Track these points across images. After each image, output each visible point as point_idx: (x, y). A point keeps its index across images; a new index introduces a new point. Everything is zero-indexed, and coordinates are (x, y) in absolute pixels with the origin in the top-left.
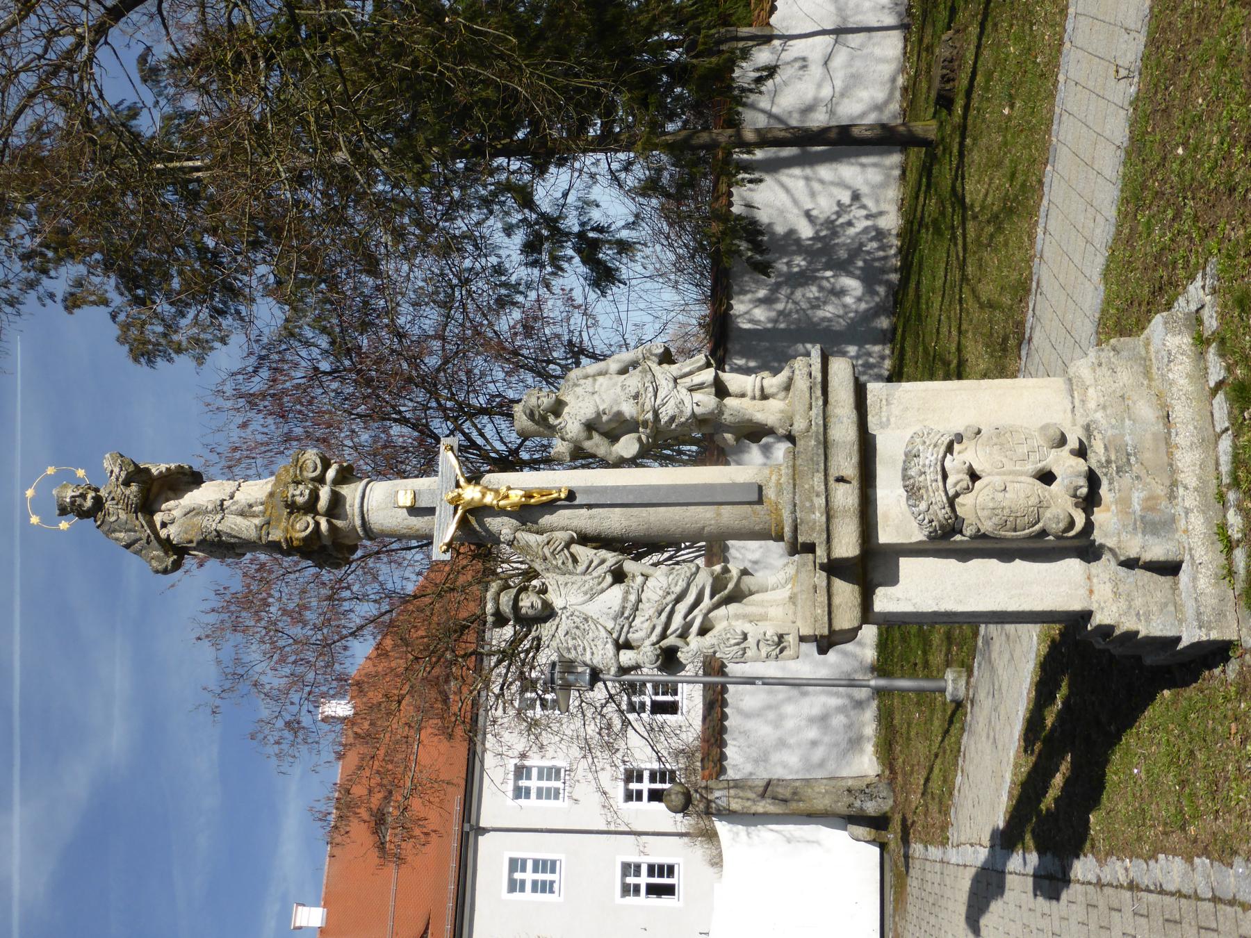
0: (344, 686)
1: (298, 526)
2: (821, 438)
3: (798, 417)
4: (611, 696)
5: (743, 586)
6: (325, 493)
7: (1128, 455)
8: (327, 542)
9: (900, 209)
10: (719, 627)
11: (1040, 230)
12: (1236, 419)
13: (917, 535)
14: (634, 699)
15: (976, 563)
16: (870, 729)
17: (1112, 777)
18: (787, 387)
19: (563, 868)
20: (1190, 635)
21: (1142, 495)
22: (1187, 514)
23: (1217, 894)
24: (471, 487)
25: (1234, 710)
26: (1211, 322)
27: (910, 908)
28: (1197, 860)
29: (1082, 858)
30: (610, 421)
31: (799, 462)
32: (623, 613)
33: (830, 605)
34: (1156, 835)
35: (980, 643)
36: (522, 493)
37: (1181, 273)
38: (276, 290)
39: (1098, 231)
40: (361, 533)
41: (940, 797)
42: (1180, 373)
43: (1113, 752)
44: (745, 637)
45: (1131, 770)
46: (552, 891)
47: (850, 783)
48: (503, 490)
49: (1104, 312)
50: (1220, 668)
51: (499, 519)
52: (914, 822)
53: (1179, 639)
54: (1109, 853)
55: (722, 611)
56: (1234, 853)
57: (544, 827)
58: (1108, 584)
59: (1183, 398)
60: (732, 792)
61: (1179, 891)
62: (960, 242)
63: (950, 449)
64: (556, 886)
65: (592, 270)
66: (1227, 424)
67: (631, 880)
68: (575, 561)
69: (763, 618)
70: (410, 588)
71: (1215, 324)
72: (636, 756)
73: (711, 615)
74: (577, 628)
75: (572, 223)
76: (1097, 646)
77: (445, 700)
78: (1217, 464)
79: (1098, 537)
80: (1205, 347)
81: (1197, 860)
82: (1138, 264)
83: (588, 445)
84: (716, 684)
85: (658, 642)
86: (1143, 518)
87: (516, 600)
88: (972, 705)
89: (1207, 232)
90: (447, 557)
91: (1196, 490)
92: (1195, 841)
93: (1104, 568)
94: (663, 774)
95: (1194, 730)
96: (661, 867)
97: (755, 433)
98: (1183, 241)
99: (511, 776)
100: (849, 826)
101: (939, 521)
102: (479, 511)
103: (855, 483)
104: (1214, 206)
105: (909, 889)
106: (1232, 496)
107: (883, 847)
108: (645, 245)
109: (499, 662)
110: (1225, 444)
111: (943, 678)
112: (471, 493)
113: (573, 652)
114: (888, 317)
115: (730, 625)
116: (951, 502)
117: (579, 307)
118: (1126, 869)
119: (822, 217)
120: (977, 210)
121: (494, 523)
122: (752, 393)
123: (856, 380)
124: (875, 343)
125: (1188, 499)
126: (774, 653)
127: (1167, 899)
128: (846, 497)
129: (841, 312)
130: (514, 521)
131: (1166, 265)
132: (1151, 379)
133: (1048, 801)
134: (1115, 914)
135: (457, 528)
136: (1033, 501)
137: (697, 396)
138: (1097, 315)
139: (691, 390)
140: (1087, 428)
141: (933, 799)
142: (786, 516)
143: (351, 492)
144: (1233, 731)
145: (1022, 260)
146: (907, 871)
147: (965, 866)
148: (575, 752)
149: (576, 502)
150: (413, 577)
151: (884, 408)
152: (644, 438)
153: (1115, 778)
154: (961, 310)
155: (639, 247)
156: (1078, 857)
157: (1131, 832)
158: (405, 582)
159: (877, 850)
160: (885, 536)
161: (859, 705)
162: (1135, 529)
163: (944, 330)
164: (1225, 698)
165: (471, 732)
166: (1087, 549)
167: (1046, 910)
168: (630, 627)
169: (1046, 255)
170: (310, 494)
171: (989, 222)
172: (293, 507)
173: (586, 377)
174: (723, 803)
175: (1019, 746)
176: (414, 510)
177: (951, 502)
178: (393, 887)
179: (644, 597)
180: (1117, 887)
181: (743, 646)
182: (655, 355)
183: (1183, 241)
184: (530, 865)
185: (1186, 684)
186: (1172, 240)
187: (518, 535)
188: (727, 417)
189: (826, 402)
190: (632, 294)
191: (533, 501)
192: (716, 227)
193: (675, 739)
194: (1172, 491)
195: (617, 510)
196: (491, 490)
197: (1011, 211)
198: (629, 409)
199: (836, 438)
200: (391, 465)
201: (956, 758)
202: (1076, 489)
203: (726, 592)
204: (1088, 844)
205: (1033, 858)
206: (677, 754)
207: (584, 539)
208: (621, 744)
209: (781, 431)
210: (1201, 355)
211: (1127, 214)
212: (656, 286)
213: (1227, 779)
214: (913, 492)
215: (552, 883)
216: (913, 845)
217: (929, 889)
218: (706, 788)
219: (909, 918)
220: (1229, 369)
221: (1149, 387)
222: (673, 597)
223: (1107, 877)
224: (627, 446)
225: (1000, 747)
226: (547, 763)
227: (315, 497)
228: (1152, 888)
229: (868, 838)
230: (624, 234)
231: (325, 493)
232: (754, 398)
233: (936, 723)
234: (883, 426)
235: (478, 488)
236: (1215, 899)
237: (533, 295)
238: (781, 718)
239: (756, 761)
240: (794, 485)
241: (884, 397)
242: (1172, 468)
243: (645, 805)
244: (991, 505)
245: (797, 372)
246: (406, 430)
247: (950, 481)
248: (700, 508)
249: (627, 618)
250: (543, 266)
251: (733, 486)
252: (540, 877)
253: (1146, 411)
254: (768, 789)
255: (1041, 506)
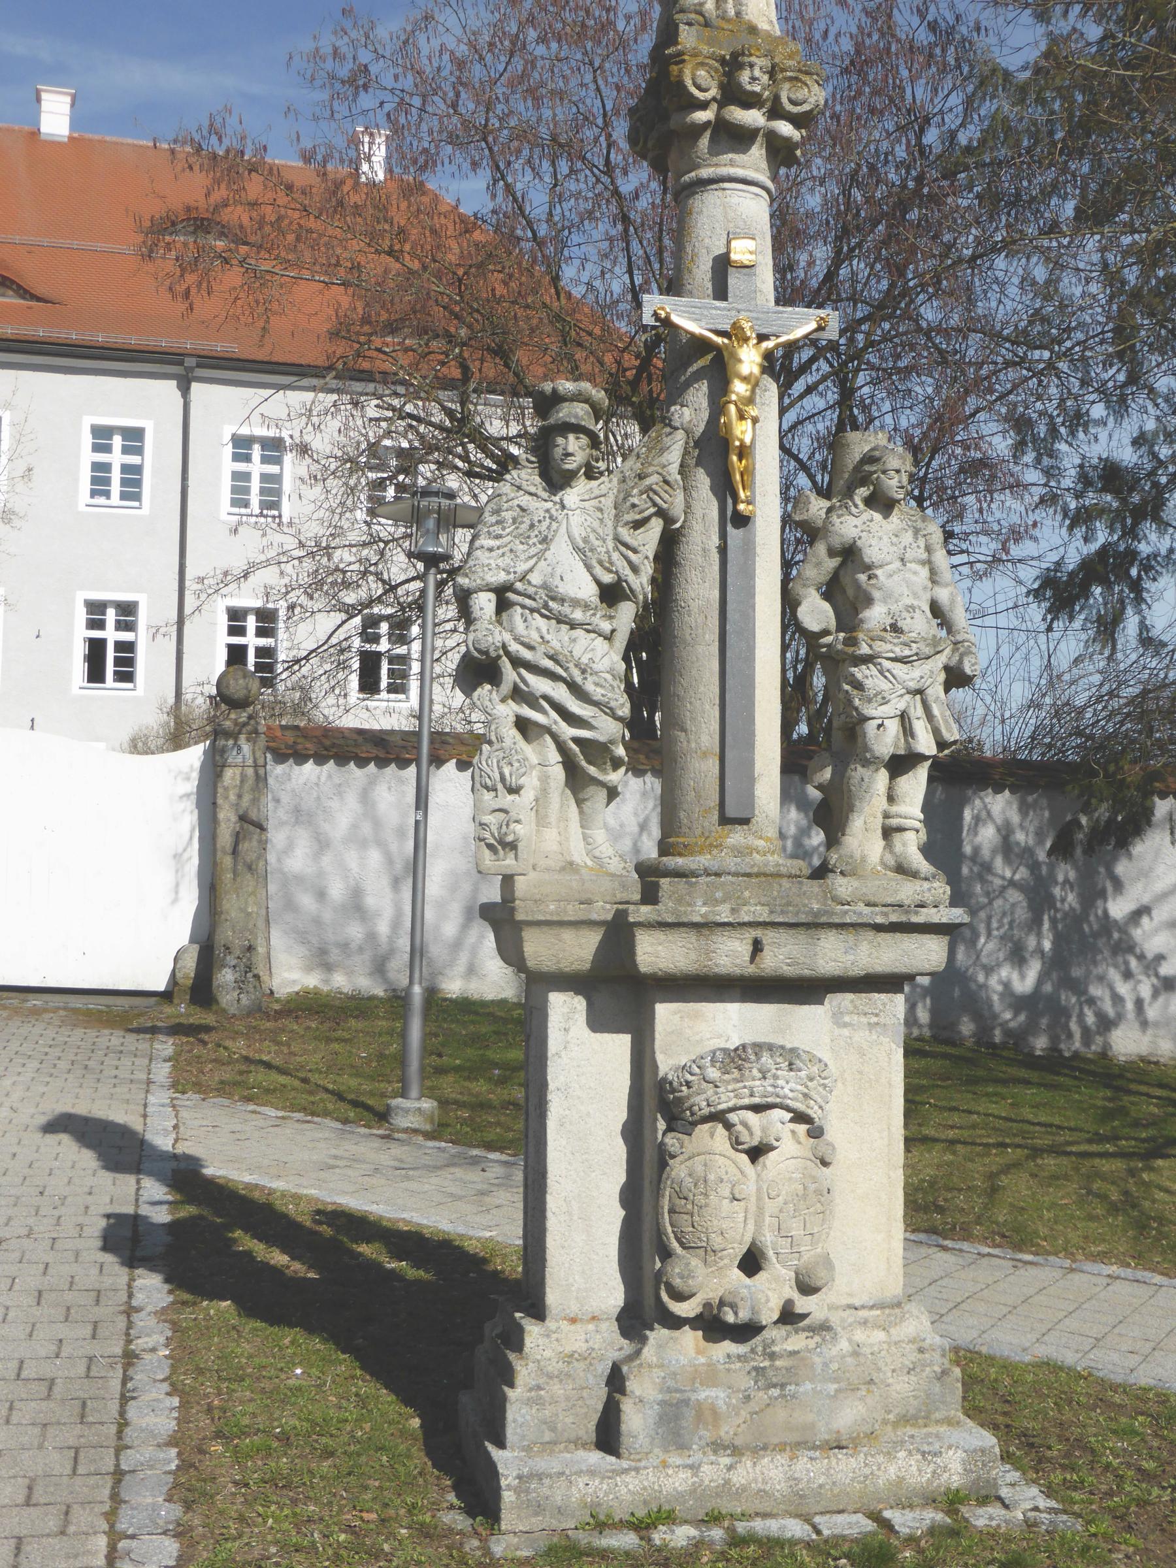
0: (412, 162)
1: (702, 73)
2: (823, 919)
3: (856, 884)
4: (393, 588)
5: (592, 790)
6: (754, 117)
7: (783, 1386)
8: (674, 123)
9: (1142, 1059)
10: (529, 751)
11: (1114, 1269)
12: (835, 1546)
13: (666, 1063)
14: (384, 627)
15: (619, 1150)
16: (340, 982)
17: (289, 1336)
18: (902, 870)
19: (130, 512)
20: (508, 1462)
21: (721, 1402)
22: (691, 1467)
23: (127, 1477)
24: (758, 359)
25: (396, 1519)
26: (982, 1518)
27: (79, 1032)
28: (174, 1451)
29: (167, 1287)
30: (857, 586)
31: (786, 883)
32: (553, 599)
33: (561, 924)
34: (206, 1396)
35: (475, 1152)
36: (748, 441)
37: (1057, 1477)
38: (1055, 57)
39: (1115, 1357)
40: (686, 178)
41: (241, 1084)
42: (904, 1468)
43: (325, 1341)
44: (514, 790)
45: (300, 1363)
46: (94, 493)
47: (261, 950)
48: (753, 411)
49: (990, 1359)
50: (456, 1502)
51: (705, 404)
52: (205, 1043)
53: (501, 1445)
54: (175, 1326)
55: (554, 756)
56: (188, 1506)
57: (191, 482)
58: (584, 1346)
59: (867, 1471)
60: (250, 771)
61: (127, 1424)
62: (1094, 1148)
63: (800, 1117)
64: (101, 500)
65: (1071, 574)
66: (826, 1533)
67: (111, 616)
68: (638, 525)
69: (541, 820)
70: (568, 272)
71: (980, 1523)
72: (302, 626)
73: (548, 738)
74: (532, 526)
75: (1152, 541)
76: (488, 1326)
77: (392, 328)
78: (765, 1515)
79: (658, 1335)
80: (945, 1506)
81: (174, 1451)
82: (1068, 1415)
83: (821, 548)
84: (418, 748)
85: (508, 653)
86: (686, 1402)
87: (578, 429)
88: (383, 1137)
89: (1122, 1518)
90: (648, 319)
91: (727, 1482)
92: (202, 1452)
93: (609, 1343)
94: (270, 668)
95: (363, 1459)
96: (130, 662)
97: (831, 815)
98: (1107, 1483)
99: (272, 433)
100: (196, 947)
101: (688, 1097)
102: (720, 371)
103: (751, 970)
104: (1163, 1530)
105: (107, 1032)
106: (717, 1533)
107: (166, 996)
108: (1110, 658)
109: (450, 413)
110: (796, 1529)
111: (422, 1095)
112: (749, 359)
113: (493, 519)
114: (974, 1035)
115: (533, 767)
116: (718, 1117)
117: (1005, 549)
118: (153, 1350)
119: (1137, 933)
120: (1145, 1176)
121: (699, 395)
122: (890, 811)
123: (910, 978)
124: (934, 1012)
125: (713, 1471)
126: (487, 835)
127: (114, 1406)
128: (730, 953)
129: (984, 960)
130: (701, 428)
131: (1067, 1455)
132: (896, 1425)
133: (246, 1242)
134: (89, 1330)
135: (693, 335)
136: (717, 1241)
137: (893, 726)
138: (984, 1349)
139: (904, 717)
140: (824, 1328)
141: (241, 1073)
142: (702, 861)
143: (753, 162)
144: (365, 1515)
145: (1067, 1241)
146: (138, 1031)
147: (145, 1116)
148: (313, 530)
149: (729, 528)
150: (585, 277)
151: (864, 1020)
152: (828, 639)
153: (287, 1341)
154: (987, 1145)
155: (1107, 653)
156: (167, 1280)
157: (209, 1359)
158: (577, 262)
159: (161, 986)
160: (665, 1013)
161: (379, 968)
162: (669, 1390)
163: (956, 1118)
164: (414, 1506)
165: (342, 369)
166: (640, 1316)
167: (87, 1231)
168: (532, 610)
169: (1077, 1277)
170: (754, 93)
171: (1126, 1193)
172: (732, 64)
173: (928, 549)
174: (233, 757)
175: (324, 1203)
176: (723, 265)
177: (718, 1117)
178: (100, 246)
179: (579, 633)
180: (128, 1334)
181: (500, 786)
182: (961, 661)
183: (1107, 1483)
184: (134, 460)
185: (430, 1451)
186: (1108, 1466)
187: (680, 435)
188: (858, 772)
189: (879, 928)
190: (1023, 635)
191: (735, 458)
192: (1132, 773)
193: (326, 686)
194: (725, 1448)
195: (716, 593)
196: (753, 391)
197: (1141, 1226)
198: (875, 616)
199: (822, 943)
200: (787, 232)
201: (304, 1109)
202: (734, 1307)
203: (584, 763)
204: (186, 1296)
205: (161, 1216)
206: (305, 690)
207: (670, 543)
208: (319, 603)
209: (834, 857)
210: (931, 1501)
211: (1146, 1401)
212: (1035, 675)
213: (295, 1502)
214: (736, 1059)
215: (107, 494)
216: (171, 1041)
217: (107, 1061)
218: (256, 732)
219: (65, 1031)
220: (911, 1540)
221: (885, 1422)
222: (579, 679)
223: (142, 1321)
224: (816, 613)
225: (322, 1175)
226: (287, 485)
227: (750, 101)
228: (129, 1385)
229: (178, 975)
230: (1131, 624)
231: (754, 117)
232: (886, 816)
233: (353, 1082)
234: (837, 1018)
235: (756, 370)
236: (119, 1475)
237: (1033, 476)
238: (363, 844)
239: (297, 811)
240: (749, 875)
241: (882, 1020)
242: (760, 1449)
243: (223, 639)
244: (712, 1177)
245: (926, 885)
246: (820, 269)
247: (750, 1116)
248: (715, 726)
249: (546, 606)
250: (1078, 496)
251: (750, 780)
252: (116, 476)
253: (849, 1415)
254: (252, 825)
255: (709, 1252)
